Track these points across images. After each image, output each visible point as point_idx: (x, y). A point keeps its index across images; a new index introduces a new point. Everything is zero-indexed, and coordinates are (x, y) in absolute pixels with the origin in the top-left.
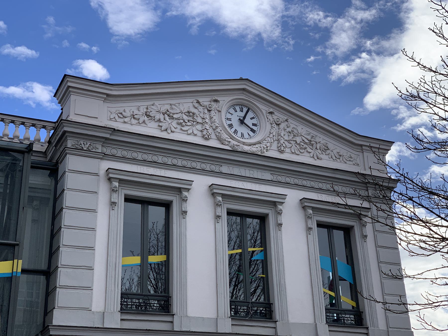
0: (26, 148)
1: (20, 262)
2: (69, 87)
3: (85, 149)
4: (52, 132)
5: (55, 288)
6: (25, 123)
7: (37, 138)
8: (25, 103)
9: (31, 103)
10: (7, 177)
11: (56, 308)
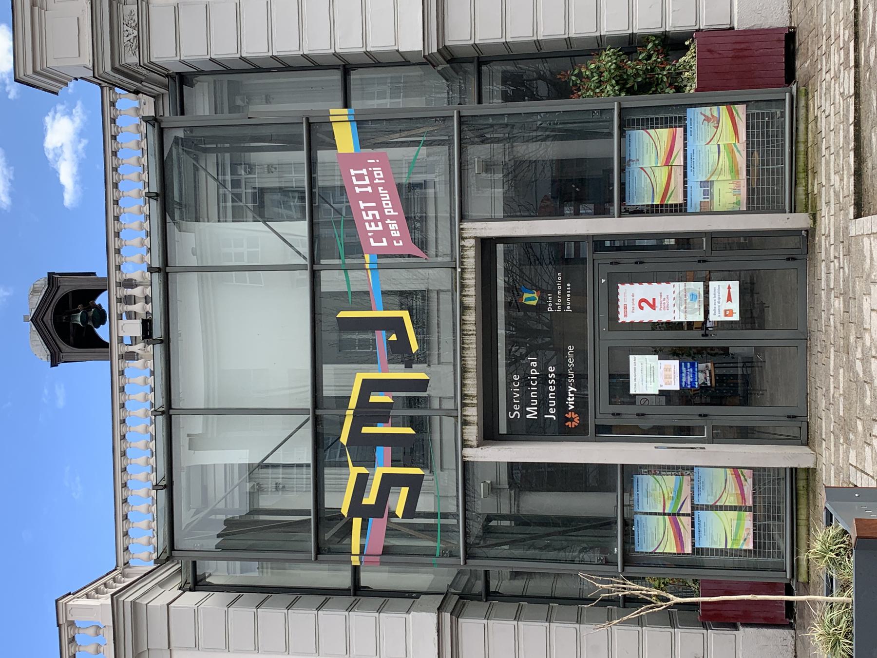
0: (154, 126)
1: (332, 111)
2: (35, 72)
3: (136, 33)
4: (117, 90)
5: (367, 53)
6: (113, 134)
7: (133, 112)
8: (84, 156)
9: (81, 146)
10: (206, 150)
11: (397, 48)
